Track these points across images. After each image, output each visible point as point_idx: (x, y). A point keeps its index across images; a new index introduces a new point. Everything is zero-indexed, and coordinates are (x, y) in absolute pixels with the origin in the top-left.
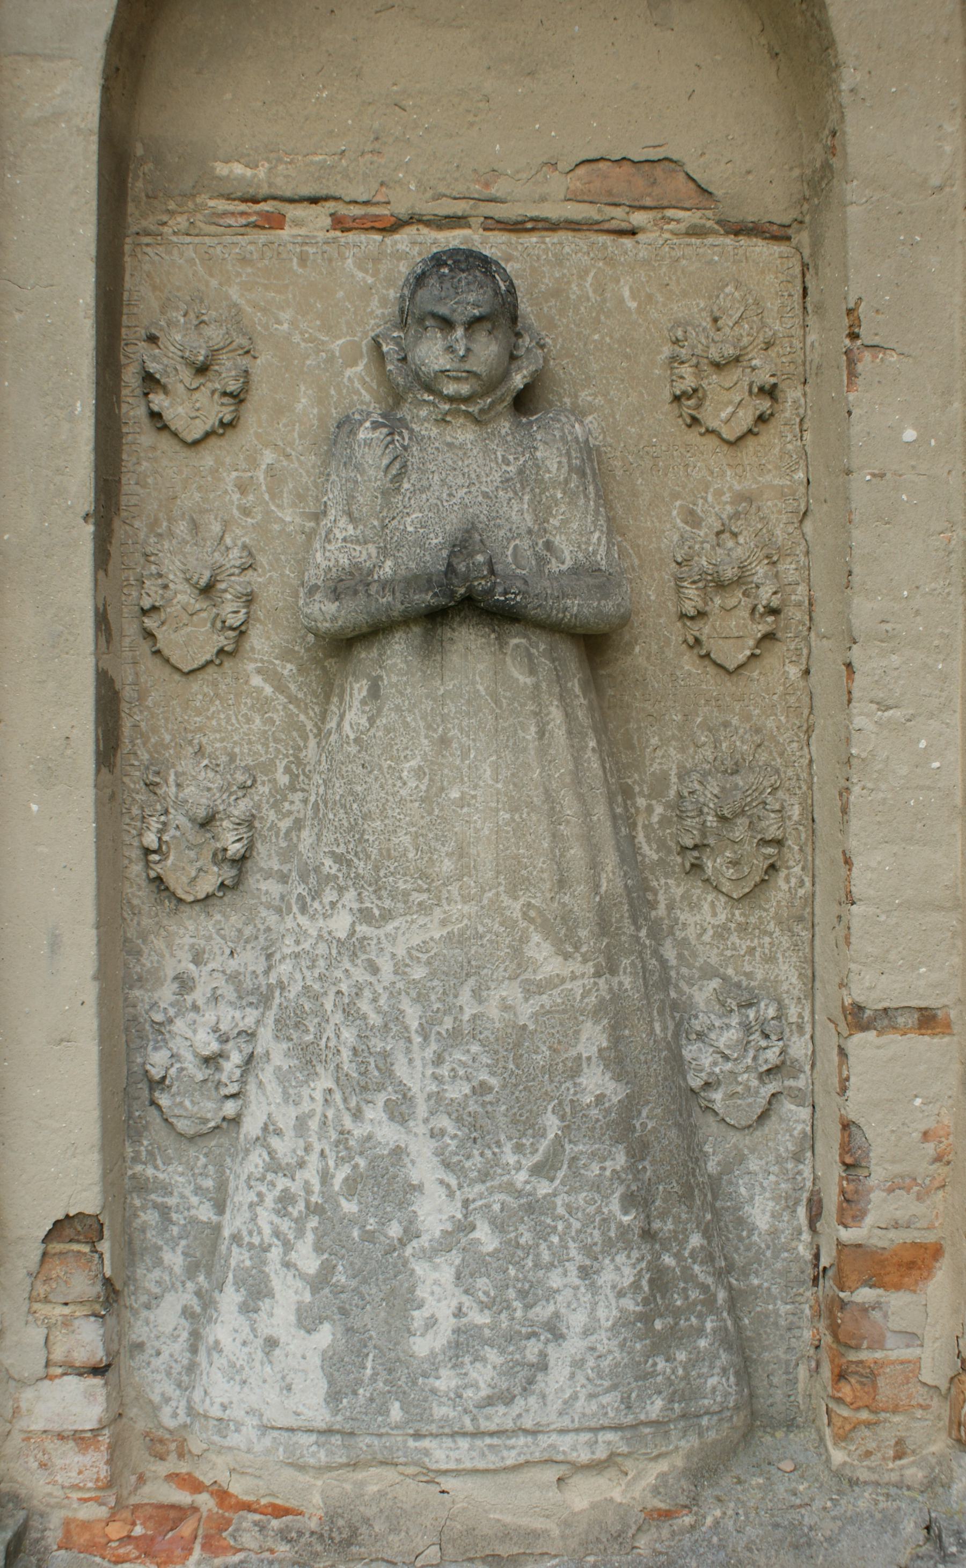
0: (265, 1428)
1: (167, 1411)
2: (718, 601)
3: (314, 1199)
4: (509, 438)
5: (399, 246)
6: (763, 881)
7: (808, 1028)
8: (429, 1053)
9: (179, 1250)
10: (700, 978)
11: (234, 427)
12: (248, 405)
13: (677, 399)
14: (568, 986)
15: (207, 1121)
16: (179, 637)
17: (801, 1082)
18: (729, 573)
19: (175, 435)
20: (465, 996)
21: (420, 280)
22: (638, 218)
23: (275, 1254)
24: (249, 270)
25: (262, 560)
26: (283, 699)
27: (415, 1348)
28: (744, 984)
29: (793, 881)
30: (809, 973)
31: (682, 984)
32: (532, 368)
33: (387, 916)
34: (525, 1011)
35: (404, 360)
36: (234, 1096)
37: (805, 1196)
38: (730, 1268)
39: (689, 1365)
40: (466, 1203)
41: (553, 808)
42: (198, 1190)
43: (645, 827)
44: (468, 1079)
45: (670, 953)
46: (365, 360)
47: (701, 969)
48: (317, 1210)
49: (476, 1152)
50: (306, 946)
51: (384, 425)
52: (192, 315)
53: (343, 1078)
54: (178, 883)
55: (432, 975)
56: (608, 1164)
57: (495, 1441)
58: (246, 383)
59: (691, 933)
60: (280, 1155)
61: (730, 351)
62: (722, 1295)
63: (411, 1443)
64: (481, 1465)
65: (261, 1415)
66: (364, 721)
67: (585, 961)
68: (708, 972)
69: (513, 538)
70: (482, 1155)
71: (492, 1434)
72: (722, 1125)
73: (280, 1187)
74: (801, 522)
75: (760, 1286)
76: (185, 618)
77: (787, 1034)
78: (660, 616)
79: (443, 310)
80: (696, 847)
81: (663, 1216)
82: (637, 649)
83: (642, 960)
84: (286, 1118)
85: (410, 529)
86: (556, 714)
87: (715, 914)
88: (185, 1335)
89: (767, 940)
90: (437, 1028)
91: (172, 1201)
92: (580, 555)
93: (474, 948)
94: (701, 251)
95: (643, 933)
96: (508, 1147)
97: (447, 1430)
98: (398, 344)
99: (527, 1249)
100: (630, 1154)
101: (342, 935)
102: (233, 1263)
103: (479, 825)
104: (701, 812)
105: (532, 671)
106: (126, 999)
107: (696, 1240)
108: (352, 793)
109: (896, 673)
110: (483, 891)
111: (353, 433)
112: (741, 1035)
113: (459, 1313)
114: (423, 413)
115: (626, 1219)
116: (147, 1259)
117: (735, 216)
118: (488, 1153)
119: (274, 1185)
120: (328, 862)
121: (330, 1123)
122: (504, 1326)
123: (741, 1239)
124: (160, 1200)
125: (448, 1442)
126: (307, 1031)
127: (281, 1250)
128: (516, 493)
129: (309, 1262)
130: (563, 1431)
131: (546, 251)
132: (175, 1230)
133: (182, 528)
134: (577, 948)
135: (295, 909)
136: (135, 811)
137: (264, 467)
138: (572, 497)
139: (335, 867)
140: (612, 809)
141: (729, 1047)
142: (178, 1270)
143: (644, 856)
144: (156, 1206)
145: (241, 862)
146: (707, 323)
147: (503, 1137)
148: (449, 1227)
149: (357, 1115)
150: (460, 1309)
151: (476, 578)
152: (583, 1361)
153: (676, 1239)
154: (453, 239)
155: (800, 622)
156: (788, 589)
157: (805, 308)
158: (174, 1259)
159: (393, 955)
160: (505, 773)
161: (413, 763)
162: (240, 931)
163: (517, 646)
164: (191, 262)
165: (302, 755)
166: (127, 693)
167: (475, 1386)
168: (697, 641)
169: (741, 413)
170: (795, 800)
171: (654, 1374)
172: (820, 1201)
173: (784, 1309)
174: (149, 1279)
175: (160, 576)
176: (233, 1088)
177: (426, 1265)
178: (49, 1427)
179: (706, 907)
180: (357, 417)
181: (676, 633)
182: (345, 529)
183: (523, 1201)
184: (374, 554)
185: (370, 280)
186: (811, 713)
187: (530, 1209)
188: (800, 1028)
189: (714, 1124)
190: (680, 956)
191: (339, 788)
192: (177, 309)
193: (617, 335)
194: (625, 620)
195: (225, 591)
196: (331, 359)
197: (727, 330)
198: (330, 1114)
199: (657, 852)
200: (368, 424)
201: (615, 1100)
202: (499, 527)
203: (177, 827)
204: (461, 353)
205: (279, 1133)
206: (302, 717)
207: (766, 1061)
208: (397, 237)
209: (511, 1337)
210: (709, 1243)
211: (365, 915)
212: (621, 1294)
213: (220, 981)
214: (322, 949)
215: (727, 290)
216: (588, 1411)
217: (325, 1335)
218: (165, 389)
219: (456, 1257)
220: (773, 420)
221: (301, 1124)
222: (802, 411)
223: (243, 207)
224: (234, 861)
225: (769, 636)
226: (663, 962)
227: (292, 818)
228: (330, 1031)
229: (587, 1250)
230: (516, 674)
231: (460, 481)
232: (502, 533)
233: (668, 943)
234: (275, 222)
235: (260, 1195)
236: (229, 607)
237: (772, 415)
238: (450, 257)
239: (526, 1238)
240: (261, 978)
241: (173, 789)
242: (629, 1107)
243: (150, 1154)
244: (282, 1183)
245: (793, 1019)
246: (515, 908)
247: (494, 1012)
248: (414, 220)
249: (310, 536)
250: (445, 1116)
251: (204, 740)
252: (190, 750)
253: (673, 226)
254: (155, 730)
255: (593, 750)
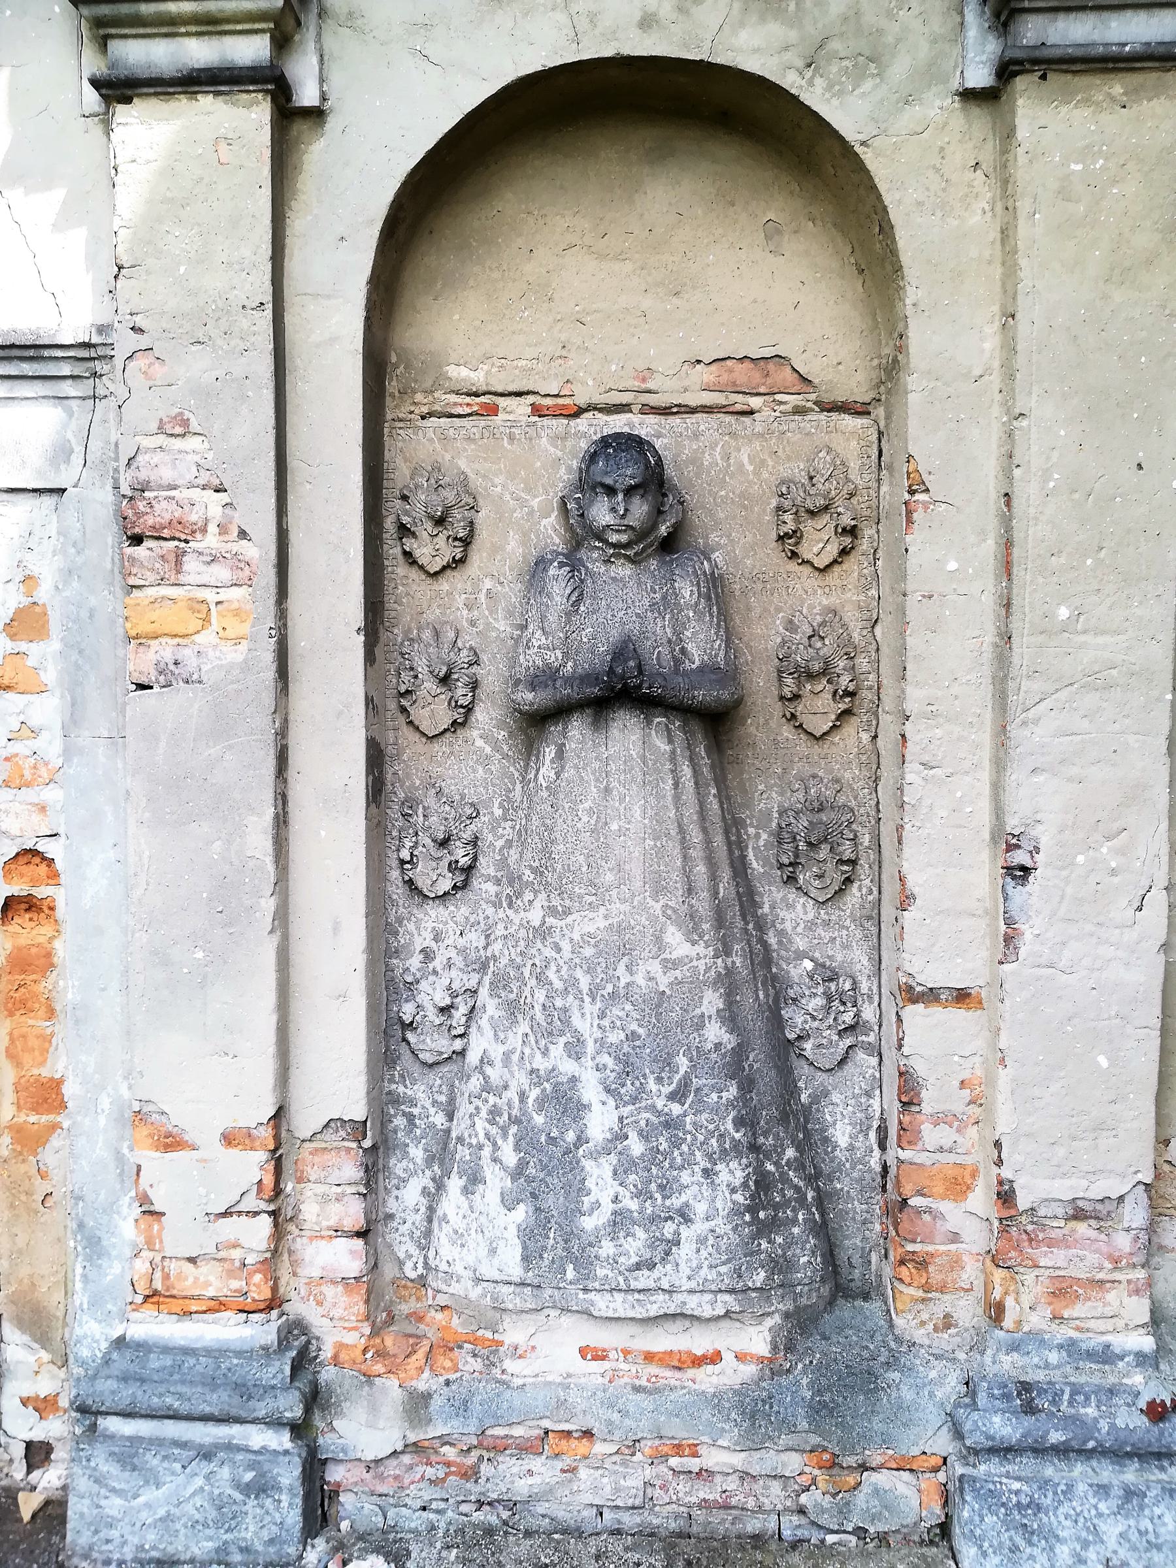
0: (478, 1280)
1: (409, 1265)
2: (808, 687)
3: (515, 1112)
4: (656, 573)
5: (580, 428)
6: (841, 889)
7: (876, 998)
8: (596, 1012)
9: (421, 1146)
10: (794, 959)
11: (464, 562)
12: (474, 547)
13: (781, 538)
14: (695, 963)
15: (442, 1053)
16: (426, 712)
17: (872, 1038)
18: (816, 666)
19: (421, 567)
20: (621, 970)
21: (592, 458)
22: (755, 402)
23: (487, 1152)
24: (473, 447)
25: (484, 657)
26: (498, 756)
27: (584, 1225)
28: (828, 964)
29: (864, 890)
30: (877, 957)
31: (781, 962)
32: (673, 521)
33: (567, 912)
34: (663, 982)
35: (582, 515)
36: (461, 1036)
37: (875, 1124)
38: (818, 1175)
39: (788, 1245)
40: (621, 1119)
41: (684, 838)
42: (435, 1103)
43: (754, 848)
44: (623, 1029)
45: (772, 940)
46: (556, 513)
47: (795, 952)
48: (517, 1121)
49: (629, 1083)
50: (512, 930)
51: (567, 565)
52: (433, 481)
53: (535, 1026)
54: (423, 883)
55: (599, 954)
56: (723, 1094)
57: (641, 1297)
58: (472, 531)
59: (788, 926)
60: (492, 1079)
61: (821, 502)
62: (810, 1195)
63: (581, 1295)
64: (631, 1314)
65: (475, 1271)
66: (552, 775)
67: (707, 947)
68: (801, 955)
69: (658, 647)
70: (632, 1084)
71: (639, 1291)
72: (812, 1068)
73: (491, 1102)
74: (873, 627)
75: (842, 1189)
76: (430, 699)
77: (860, 1002)
78: (766, 697)
79: (609, 481)
80: (791, 864)
81: (766, 1134)
82: (749, 721)
83: (750, 946)
84: (496, 1052)
85: (585, 640)
86: (686, 771)
87: (806, 913)
88: (423, 1209)
89: (845, 932)
90: (600, 992)
91: (416, 1111)
92: (706, 658)
93: (627, 936)
94: (802, 425)
95: (751, 926)
96: (651, 1080)
97: (607, 1287)
98: (578, 503)
99: (665, 1155)
100: (740, 1088)
101: (537, 923)
102: (458, 1157)
103: (631, 849)
104: (795, 838)
105: (670, 741)
106: (387, 965)
107: (790, 1153)
108: (544, 824)
109: (938, 742)
110: (634, 895)
111: (545, 570)
112: (825, 1002)
113: (616, 1200)
114: (595, 555)
115: (737, 1136)
116: (398, 1152)
117: (827, 398)
118: (637, 1084)
119: (487, 1102)
120: (527, 872)
121: (526, 1058)
122: (649, 1212)
123: (827, 1153)
124: (408, 1110)
125: (608, 1296)
126: (512, 992)
127: (491, 1148)
128: (660, 614)
129: (510, 1157)
130: (691, 1292)
131: (687, 428)
132: (418, 1132)
133: (427, 635)
134: (701, 937)
135: (505, 905)
136: (395, 833)
137: (484, 591)
138: (699, 615)
139: (532, 876)
140: (728, 838)
141: (815, 1010)
142: (419, 1161)
143: (753, 869)
144: (404, 1114)
145: (469, 870)
146: (805, 481)
147: (647, 1071)
148: (609, 1136)
149: (545, 1053)
150: (617, 1197)
151: (630, 678)
152: (706, 1239)
153: (776, 1151)
154: (618, 424)
155: (870, 700)
156: (862, 677)
157: (880, 465)
158: (417, 1153)
159: (572, 940)
160: (650, 812)
161: (587, 805)
162: (467, 918)
163: (659, 723)
164: (431, 440)
165: (511, 796)
166: (390, 750)
167: (626, 1254)
168: (793, 716)
169: (829, 547)
170: (865, 830)
171: (759, 1252)
172: (886, 1127)
173: (859, 1207)
174: (398, 1167)
175: (412, 669)
176: (461, 1030)
177: (593, 1163)
178: (324, 1274)
179: (799, 907)
180: (549, 557)
181: (777, 709)
182: (539, 639)
183: (662, 1119)
184: (560, 657)
185: (560, 454)
186: (878, 767)
187: (667, 1125)
188: (870, 997)
189: (806, 1066)
190: (780, 942)
191: (535, 822)
192: (422, 476)
193: (737, 492)
194: (738, 703)
195: (458, 680)
196: (531, 513)
197: (820, 486)
198: (527, 1051)
199: (763, 867)
200: (556, 564)
201: (729, 1047)
202: (647, 639)
203: (424, 846)
204: (622, 512)
205: (491, 1063)
206: (512, 769)
207: (844, 1022)
208: (578, 420)
209: (653, 1219)
210: (801, 1155)
211: (552, 911)
212: (733, 1191)
213: (452, 953)
214: (522, 933)
215: (821, 455)
216: (709, 1277)
217: (521, 1213)
218: (414, 535)
219: (613, 1158)
220: (853, 552)
221: (507, 1056)
222: (875, 544)
223: (468, 400)
224: (463, 870)
225: (847, 713)
226: (765, 945)
227: (504, 839)
228: (527, 992)
229: (709, 1156)
230: (658, 743)
231: (620, 605)
232: (649, 643)
233: (771, 933)
234: (493, 410)
235: (477, 1108)
236: (460, 692)
237: (852, 548)
238: (614, 441)
239: (664, 1146)
240: (482, 952)
241: (421, 818)
242: (740, 1052)
243: (402, 1076)
244: (492, 1099)
245: (865, 990)
246: (657, 907)
247: (640, 979)
248: (591, 408)
249: (517, 641)
250: (606, 1056)
251: (443, 784)
252: (434, 791)
253: (782, 408)
254: (408, 776)
255: (714, 795)
